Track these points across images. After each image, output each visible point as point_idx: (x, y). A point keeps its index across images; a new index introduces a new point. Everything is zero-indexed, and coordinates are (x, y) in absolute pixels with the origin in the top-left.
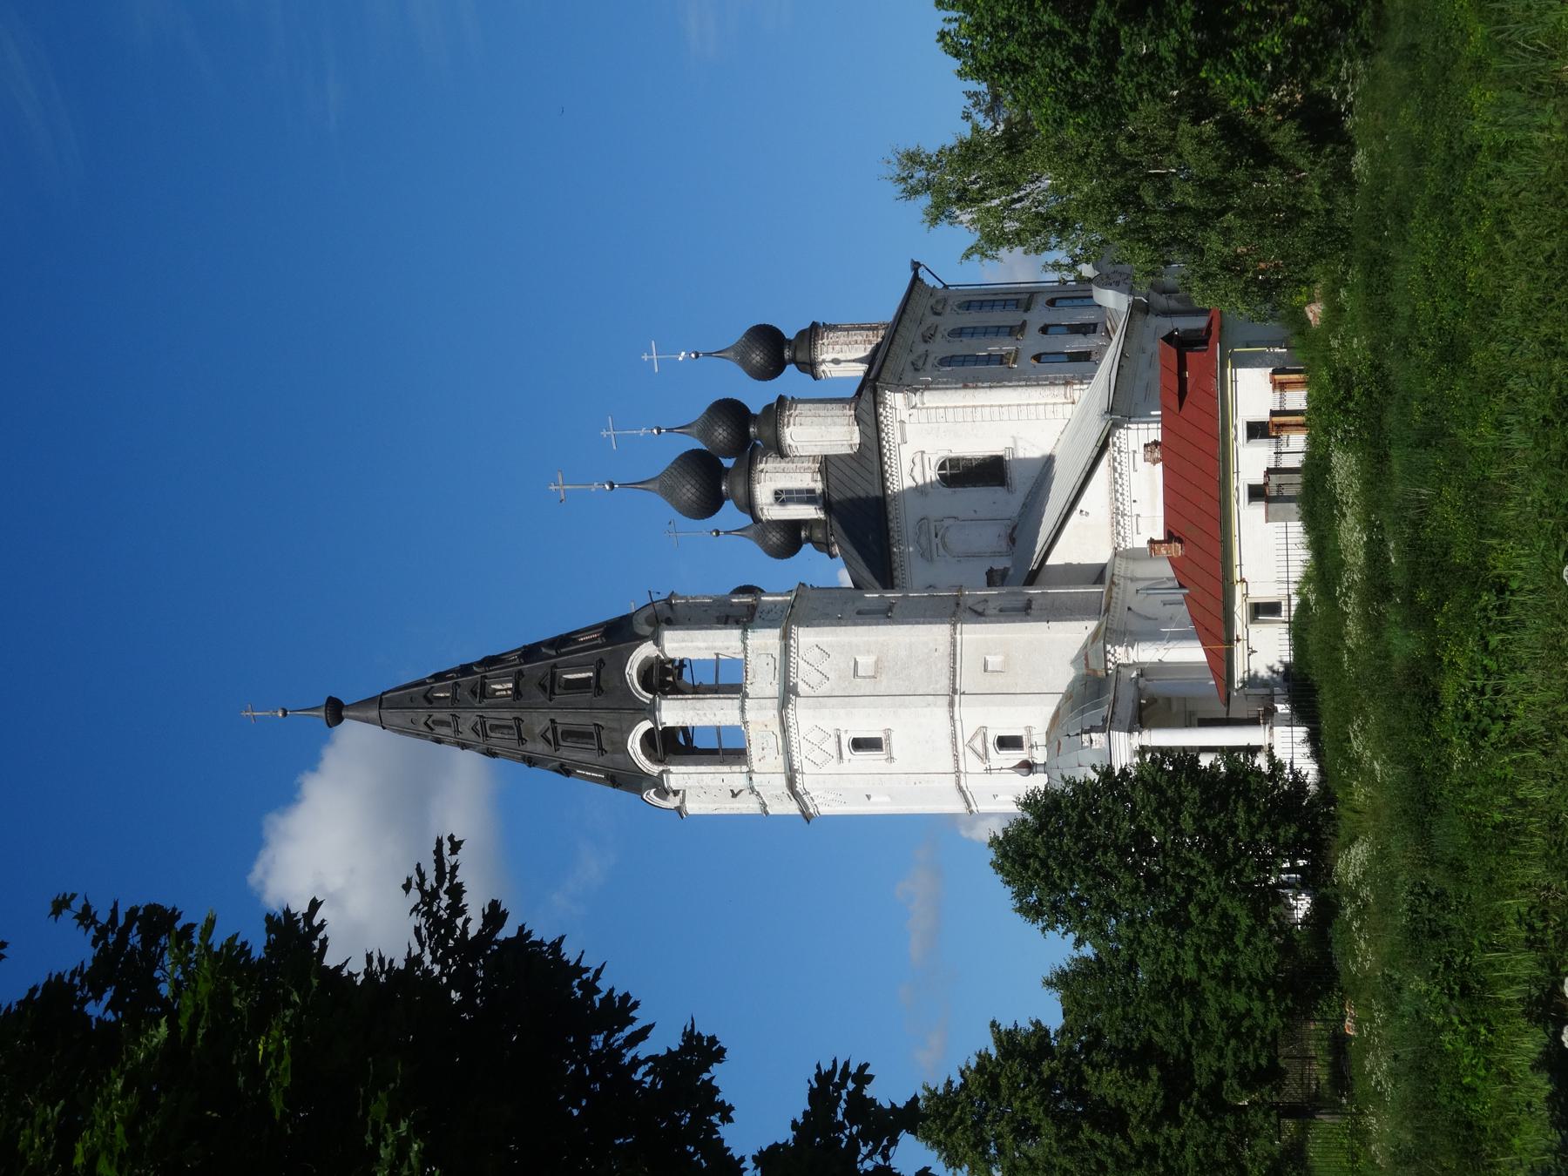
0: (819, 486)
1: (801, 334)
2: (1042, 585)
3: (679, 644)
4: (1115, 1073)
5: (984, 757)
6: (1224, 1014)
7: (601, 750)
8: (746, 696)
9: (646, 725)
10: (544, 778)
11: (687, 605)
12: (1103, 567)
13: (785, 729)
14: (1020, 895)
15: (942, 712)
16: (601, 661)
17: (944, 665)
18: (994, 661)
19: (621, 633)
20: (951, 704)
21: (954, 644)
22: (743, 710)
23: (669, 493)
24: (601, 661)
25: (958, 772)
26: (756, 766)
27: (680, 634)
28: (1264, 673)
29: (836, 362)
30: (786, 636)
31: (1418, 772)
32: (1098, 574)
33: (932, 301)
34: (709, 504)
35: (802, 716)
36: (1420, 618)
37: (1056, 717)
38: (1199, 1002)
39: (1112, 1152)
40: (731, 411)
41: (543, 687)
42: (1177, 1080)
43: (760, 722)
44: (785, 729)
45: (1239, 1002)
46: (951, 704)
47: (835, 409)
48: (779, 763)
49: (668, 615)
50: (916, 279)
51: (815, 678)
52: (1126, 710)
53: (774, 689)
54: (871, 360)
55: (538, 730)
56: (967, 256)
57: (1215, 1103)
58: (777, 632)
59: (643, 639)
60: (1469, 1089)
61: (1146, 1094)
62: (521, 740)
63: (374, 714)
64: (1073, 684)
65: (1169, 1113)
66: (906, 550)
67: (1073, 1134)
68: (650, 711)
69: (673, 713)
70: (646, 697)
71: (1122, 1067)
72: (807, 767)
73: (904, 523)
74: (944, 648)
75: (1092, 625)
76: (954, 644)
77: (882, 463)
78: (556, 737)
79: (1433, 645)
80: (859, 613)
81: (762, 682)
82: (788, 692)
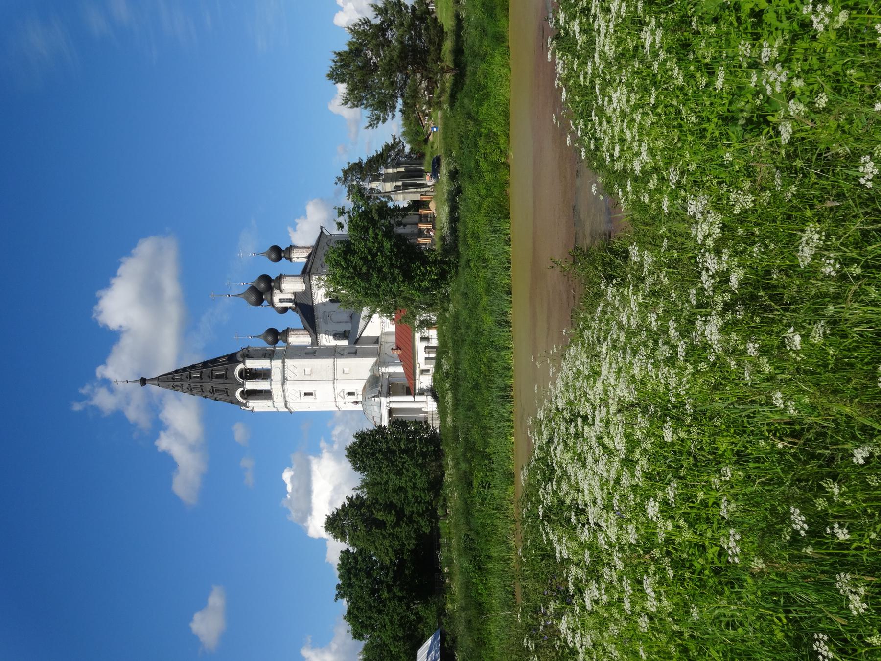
0: (293, 298)
1: (287, 249)
2: (359, 344)
3: (251, 364)
4: (382, 513)
5: (344, 398)
6: (413, 496)
7: (228, 395)
8: (271, 381)
9: (241, 389)
10: (210, 401)
11: (253, 350)
12: (378, 338)
13: (284, 391)
14: (354, 465)
15: (332, 385)
16: (227, 369)
17: (332, 371)
18: (346, 370)
19: (232, 359)
20: (334, 383)
21: (334, 365)
22: (271, 385)
23: (247, 299)
24: (227, 369)
25: (336, 402)
26: (275, 400)
27: (251, 361)
28: (425, 388)
29: (297, 258)
30: (283, 362)
31: (467, 504)
32: (376, 340)
33: (326, 241)
34: (259, 302)
35: (289, 386)
36: (469, 461)
37: (364, 387)
38: (406, 492)
39: (382, 534)
40: (266, 278)
41: (209, 376)
42: (400, 514)
43: (276, 388)
44: (284, 391)
45: (417, 493)
46: (334, 383)
47: (297, 279)
48: (282, 399)
49: (248, 355)
50: (322, 232)
51: (292, 375)
52: (385, 389)
53: (280, 378)
54: (309, 257)
55: (208, 389)
56: (337, 599)
57: (410, 520)
58: (281, 361)
59: (240, 362)
60: (480, 594)
61: (391, 518)
62: (203, 392)
63: (156, 382)
64: (370, 377)
65: (397, 524)
66: (319, 321)
67: (370, 530)
68: (242, 385)
69: (250, 385)
70: (241, 381)
71: (385, 511)
72: (291, 401)
73: (319, 313)
74: (331, 366)
75: (375, 359)
76: (334, 365)
77: (312, 296)
78: (213, 391)
79: (471, 469)
80: (306, 354)
81: (276, 375)
82: (284, 380)
